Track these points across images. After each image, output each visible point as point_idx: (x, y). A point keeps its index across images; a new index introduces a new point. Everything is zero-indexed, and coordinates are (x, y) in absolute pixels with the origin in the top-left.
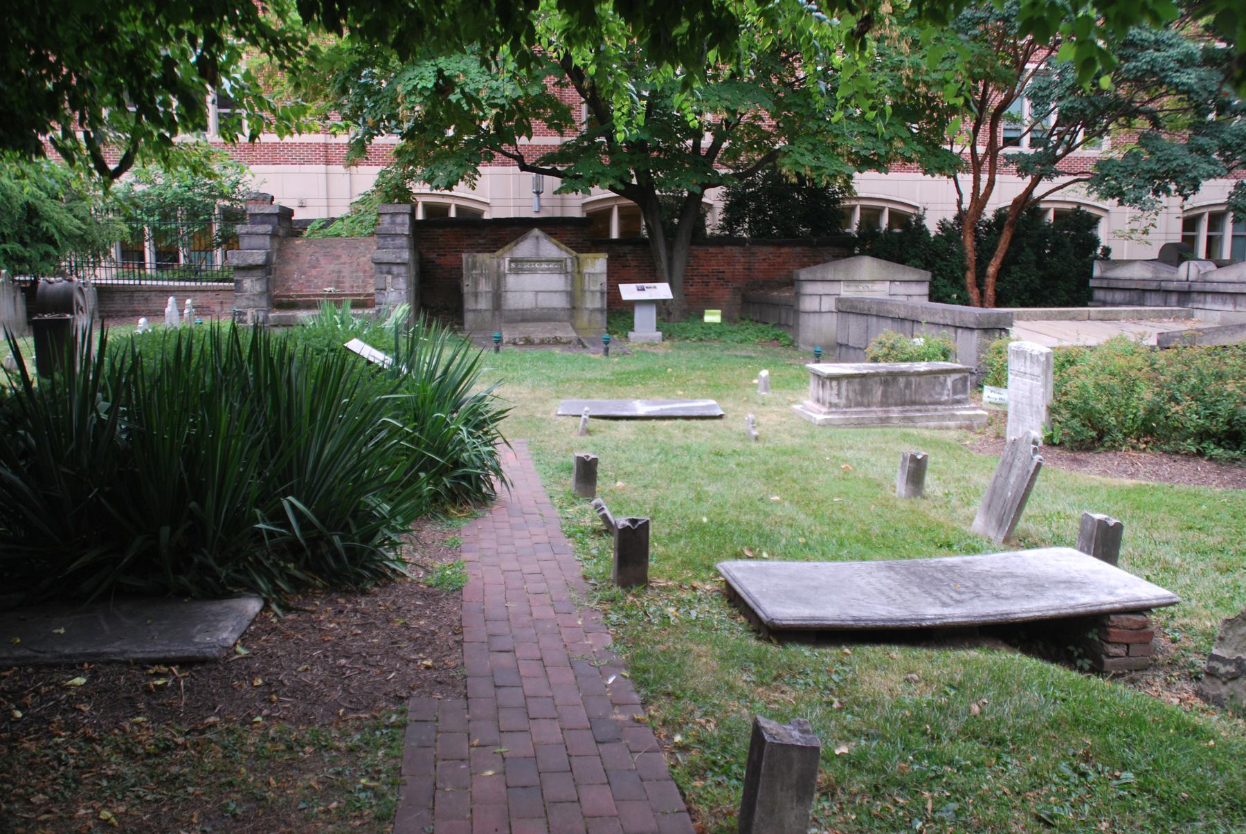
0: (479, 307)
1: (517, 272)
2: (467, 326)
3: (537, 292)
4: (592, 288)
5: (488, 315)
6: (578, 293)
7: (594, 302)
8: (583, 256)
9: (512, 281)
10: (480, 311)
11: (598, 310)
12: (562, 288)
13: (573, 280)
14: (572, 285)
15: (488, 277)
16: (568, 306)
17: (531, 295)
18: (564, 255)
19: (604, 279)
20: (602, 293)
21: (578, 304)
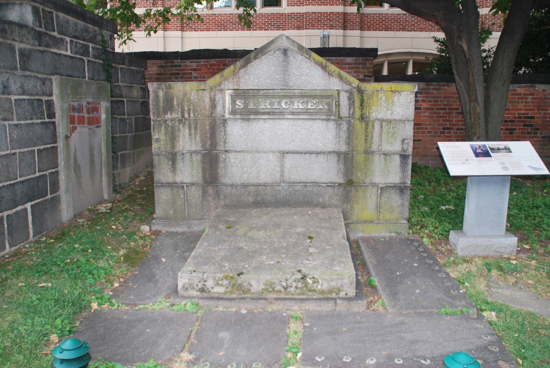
0: (179, 179)
1: (247, 114)
2: (159, 211)
3: (284, 153)
4: (387, 148)
5: (195, 194)
6: (360, 158)
7: (388, 171)
8: (371, 87)
9: (236, 133)
10: (181, 186)
11: (394, 187)
12: (331, 147)
13: (350, 131)
14: (349, 141)
15: (194, 126)
16: (340, 179)
17: (273, 159)
18: (335, 84)
19: (408, 130)
20: (404, 157)
21: (358, 176)
